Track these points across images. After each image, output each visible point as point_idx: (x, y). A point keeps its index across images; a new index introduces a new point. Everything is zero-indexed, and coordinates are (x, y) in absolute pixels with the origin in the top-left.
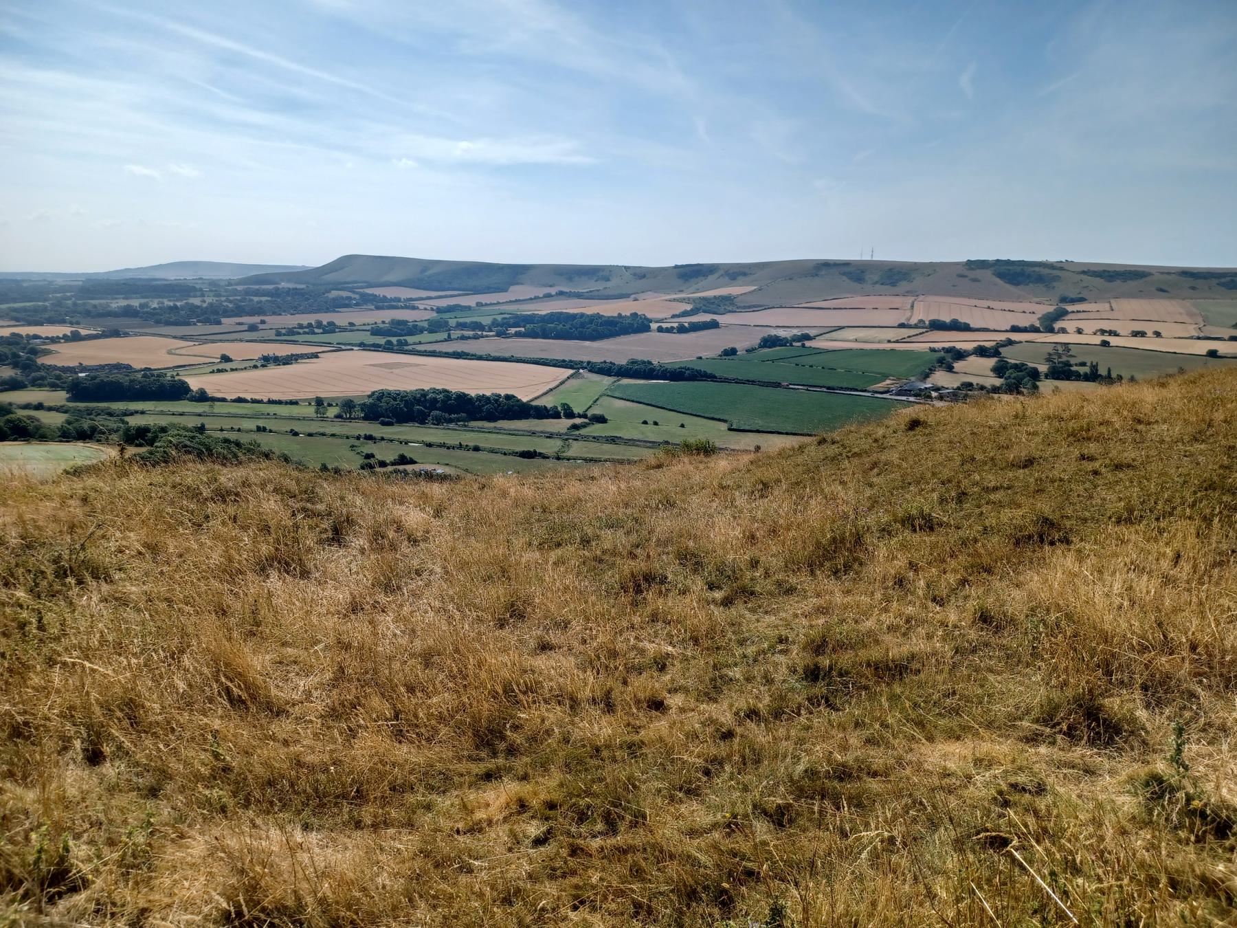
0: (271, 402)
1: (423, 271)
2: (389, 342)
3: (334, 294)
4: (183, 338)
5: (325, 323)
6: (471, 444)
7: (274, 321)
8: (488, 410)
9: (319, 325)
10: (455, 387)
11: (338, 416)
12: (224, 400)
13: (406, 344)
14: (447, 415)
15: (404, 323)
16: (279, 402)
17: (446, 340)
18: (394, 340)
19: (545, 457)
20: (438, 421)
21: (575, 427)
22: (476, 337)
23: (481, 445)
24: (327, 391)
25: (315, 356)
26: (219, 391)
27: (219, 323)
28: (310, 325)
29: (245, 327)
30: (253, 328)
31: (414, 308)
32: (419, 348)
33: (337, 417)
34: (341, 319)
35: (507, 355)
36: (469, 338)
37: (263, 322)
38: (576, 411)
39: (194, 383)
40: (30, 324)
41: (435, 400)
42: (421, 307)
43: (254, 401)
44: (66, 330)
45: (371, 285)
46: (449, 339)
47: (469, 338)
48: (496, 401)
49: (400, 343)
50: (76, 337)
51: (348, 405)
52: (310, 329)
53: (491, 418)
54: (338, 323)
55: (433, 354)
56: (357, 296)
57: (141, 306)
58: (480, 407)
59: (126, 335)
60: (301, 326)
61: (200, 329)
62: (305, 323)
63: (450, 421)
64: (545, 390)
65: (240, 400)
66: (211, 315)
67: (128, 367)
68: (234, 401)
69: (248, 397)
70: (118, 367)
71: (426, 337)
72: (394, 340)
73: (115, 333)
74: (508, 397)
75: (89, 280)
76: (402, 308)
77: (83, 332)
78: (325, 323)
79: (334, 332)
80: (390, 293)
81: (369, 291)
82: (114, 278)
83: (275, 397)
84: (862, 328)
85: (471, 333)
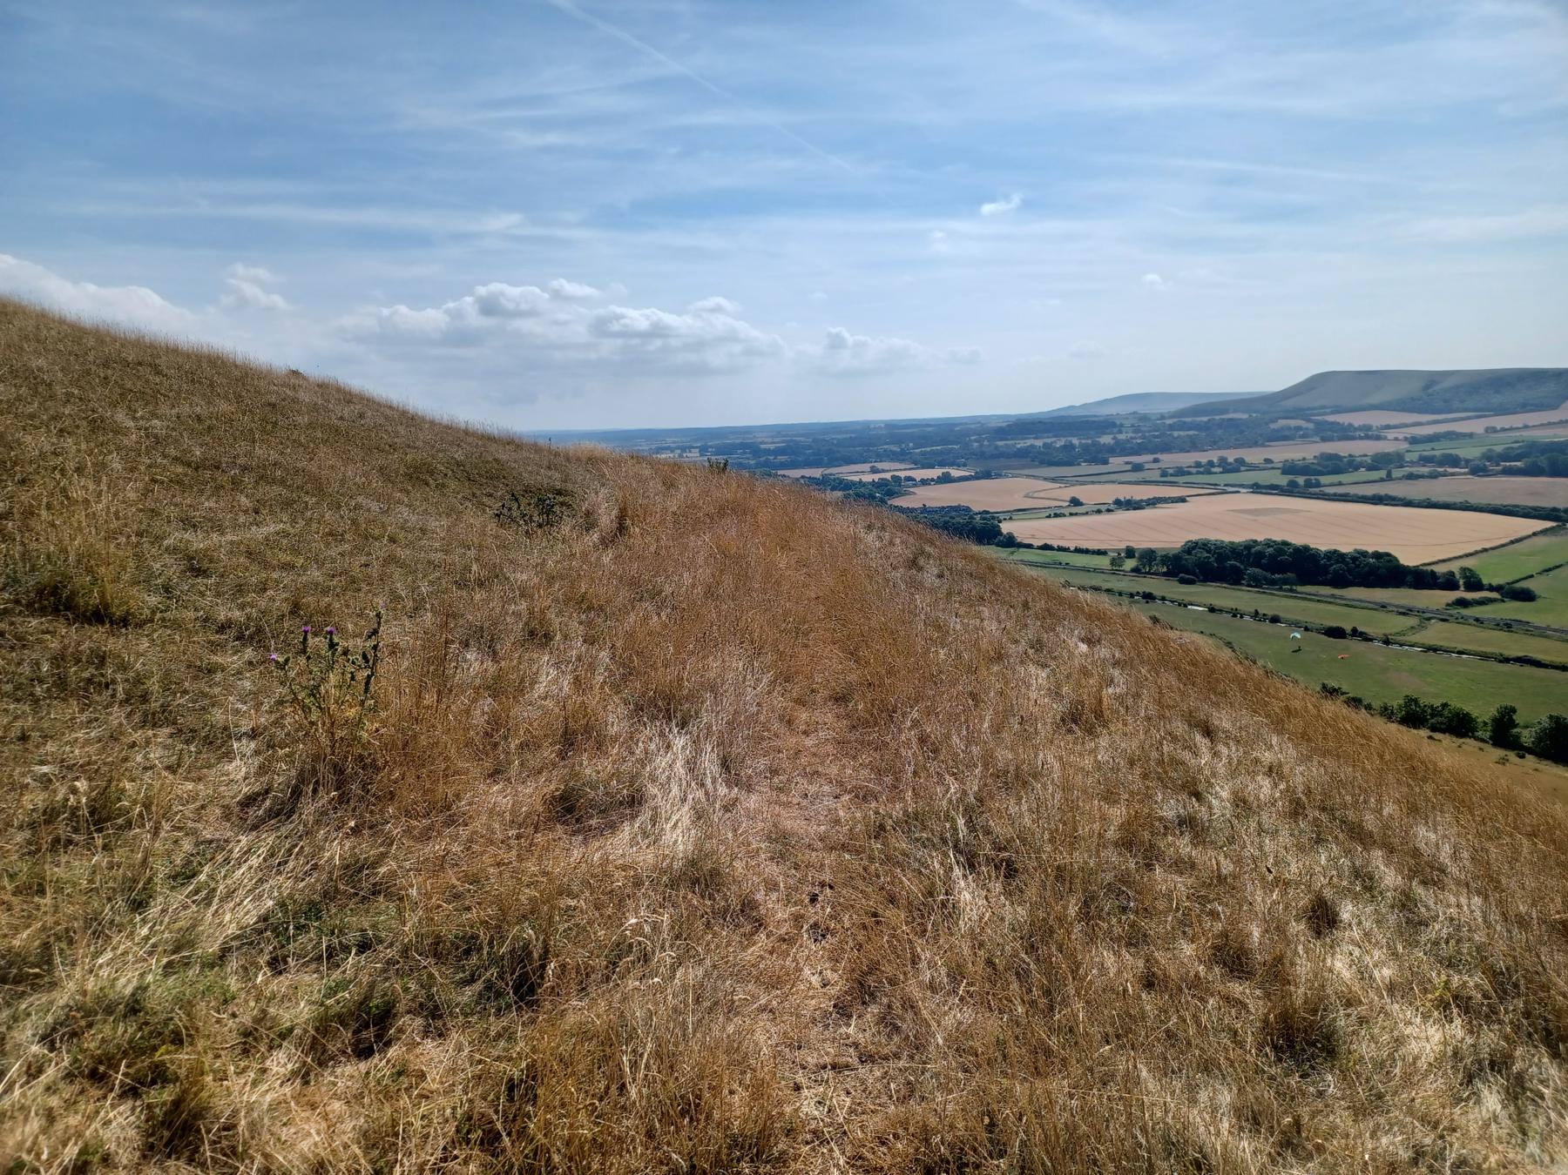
0: (1078, 551)
1: (1427, 387)
2: (1293, 484)
3: (1282, 423)
4: (1054, 480)
5: (1231, 460)
6: (1270, 613)
7: (1170, 460)
8: (1336, 572)
9: (1223, 461)
10: (1298, 538)
11: (1135, 570)
12: (1029, 546)
13: (1318, 485)
14: (1268, 575)
15: (1336, 457)
16: (1087, 551)
17: (1382, 480)
18: (1301, 480)
19: (1366, 638)
20: (1256, 583)
21: (1462, 603)
22: (1433, 476)
23: (1282, 615)
24: (1142, 542)
25: (1182, 500)
26: (1033, 537)
27: (1106, 462)
28: (1211, 463)
29: (1129, 467)
30: (1137, 468)
31: (1378, 438)
32: (1352, 490)
33: (1133, 570)
34: (1253, 456)
35: (1458, 500)
36: (1422, 477)
37: (1156, 461)
38: (1485, 581)
39: (1006, 527)
40: (924, 467)
41: (1260, 555)
42: (1390, 436)
43: (1061, 549)
44: (936, 473)
45: (1339, 410)
46: (1389, 478)
47: (1422, 477)
48: (1354, 559)
49: (1308, 484)
50: (946, 479)
51: (1149, 556)
52: (1207, 468)
53: (1340, 581)
54: (1248, 460)
55: (1345, 498)
56: (1311, 426)
57: (1045, 445)
58: (1326, 567)
59: (999, 476)
60: (1198, 465)
61: (1085, 468)
62: (1204, 461)
63: (1272, 583)
64: (1479, 548)
65: (1046, 547)
66: (1097, 456)
67: (968, 509)
68: (1040, 548)
69: (1055, 544)
70: (957, 509)
71: (1363, 474)
72: (1301, 480)
73: (987, 475)
74: (1377, 555)
75: (1197, 411)
76: (1361, 438)
77: (955, 473)
78: (1231, 460)
79: (1238, 471)
80: (1356, 419)
81: (1331, 418)
82: (1073, 413)
83: (1084, 545)
84: (601, 448)
85: (1425, 470)
